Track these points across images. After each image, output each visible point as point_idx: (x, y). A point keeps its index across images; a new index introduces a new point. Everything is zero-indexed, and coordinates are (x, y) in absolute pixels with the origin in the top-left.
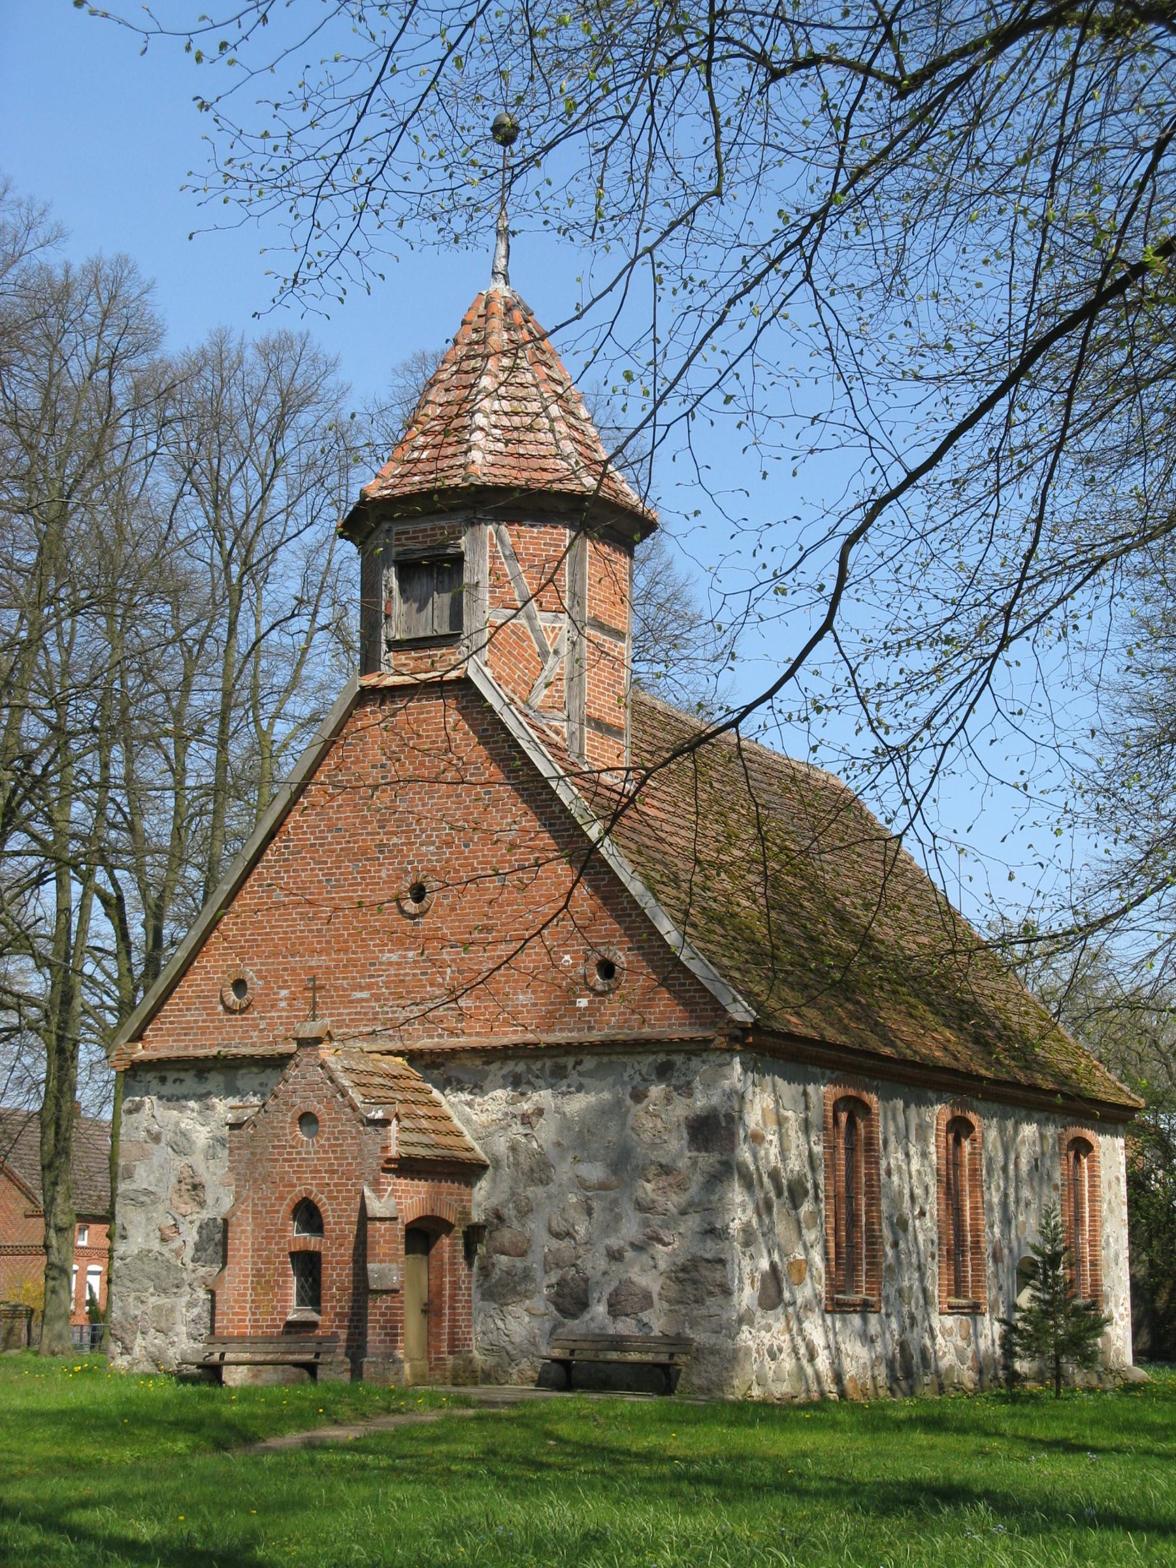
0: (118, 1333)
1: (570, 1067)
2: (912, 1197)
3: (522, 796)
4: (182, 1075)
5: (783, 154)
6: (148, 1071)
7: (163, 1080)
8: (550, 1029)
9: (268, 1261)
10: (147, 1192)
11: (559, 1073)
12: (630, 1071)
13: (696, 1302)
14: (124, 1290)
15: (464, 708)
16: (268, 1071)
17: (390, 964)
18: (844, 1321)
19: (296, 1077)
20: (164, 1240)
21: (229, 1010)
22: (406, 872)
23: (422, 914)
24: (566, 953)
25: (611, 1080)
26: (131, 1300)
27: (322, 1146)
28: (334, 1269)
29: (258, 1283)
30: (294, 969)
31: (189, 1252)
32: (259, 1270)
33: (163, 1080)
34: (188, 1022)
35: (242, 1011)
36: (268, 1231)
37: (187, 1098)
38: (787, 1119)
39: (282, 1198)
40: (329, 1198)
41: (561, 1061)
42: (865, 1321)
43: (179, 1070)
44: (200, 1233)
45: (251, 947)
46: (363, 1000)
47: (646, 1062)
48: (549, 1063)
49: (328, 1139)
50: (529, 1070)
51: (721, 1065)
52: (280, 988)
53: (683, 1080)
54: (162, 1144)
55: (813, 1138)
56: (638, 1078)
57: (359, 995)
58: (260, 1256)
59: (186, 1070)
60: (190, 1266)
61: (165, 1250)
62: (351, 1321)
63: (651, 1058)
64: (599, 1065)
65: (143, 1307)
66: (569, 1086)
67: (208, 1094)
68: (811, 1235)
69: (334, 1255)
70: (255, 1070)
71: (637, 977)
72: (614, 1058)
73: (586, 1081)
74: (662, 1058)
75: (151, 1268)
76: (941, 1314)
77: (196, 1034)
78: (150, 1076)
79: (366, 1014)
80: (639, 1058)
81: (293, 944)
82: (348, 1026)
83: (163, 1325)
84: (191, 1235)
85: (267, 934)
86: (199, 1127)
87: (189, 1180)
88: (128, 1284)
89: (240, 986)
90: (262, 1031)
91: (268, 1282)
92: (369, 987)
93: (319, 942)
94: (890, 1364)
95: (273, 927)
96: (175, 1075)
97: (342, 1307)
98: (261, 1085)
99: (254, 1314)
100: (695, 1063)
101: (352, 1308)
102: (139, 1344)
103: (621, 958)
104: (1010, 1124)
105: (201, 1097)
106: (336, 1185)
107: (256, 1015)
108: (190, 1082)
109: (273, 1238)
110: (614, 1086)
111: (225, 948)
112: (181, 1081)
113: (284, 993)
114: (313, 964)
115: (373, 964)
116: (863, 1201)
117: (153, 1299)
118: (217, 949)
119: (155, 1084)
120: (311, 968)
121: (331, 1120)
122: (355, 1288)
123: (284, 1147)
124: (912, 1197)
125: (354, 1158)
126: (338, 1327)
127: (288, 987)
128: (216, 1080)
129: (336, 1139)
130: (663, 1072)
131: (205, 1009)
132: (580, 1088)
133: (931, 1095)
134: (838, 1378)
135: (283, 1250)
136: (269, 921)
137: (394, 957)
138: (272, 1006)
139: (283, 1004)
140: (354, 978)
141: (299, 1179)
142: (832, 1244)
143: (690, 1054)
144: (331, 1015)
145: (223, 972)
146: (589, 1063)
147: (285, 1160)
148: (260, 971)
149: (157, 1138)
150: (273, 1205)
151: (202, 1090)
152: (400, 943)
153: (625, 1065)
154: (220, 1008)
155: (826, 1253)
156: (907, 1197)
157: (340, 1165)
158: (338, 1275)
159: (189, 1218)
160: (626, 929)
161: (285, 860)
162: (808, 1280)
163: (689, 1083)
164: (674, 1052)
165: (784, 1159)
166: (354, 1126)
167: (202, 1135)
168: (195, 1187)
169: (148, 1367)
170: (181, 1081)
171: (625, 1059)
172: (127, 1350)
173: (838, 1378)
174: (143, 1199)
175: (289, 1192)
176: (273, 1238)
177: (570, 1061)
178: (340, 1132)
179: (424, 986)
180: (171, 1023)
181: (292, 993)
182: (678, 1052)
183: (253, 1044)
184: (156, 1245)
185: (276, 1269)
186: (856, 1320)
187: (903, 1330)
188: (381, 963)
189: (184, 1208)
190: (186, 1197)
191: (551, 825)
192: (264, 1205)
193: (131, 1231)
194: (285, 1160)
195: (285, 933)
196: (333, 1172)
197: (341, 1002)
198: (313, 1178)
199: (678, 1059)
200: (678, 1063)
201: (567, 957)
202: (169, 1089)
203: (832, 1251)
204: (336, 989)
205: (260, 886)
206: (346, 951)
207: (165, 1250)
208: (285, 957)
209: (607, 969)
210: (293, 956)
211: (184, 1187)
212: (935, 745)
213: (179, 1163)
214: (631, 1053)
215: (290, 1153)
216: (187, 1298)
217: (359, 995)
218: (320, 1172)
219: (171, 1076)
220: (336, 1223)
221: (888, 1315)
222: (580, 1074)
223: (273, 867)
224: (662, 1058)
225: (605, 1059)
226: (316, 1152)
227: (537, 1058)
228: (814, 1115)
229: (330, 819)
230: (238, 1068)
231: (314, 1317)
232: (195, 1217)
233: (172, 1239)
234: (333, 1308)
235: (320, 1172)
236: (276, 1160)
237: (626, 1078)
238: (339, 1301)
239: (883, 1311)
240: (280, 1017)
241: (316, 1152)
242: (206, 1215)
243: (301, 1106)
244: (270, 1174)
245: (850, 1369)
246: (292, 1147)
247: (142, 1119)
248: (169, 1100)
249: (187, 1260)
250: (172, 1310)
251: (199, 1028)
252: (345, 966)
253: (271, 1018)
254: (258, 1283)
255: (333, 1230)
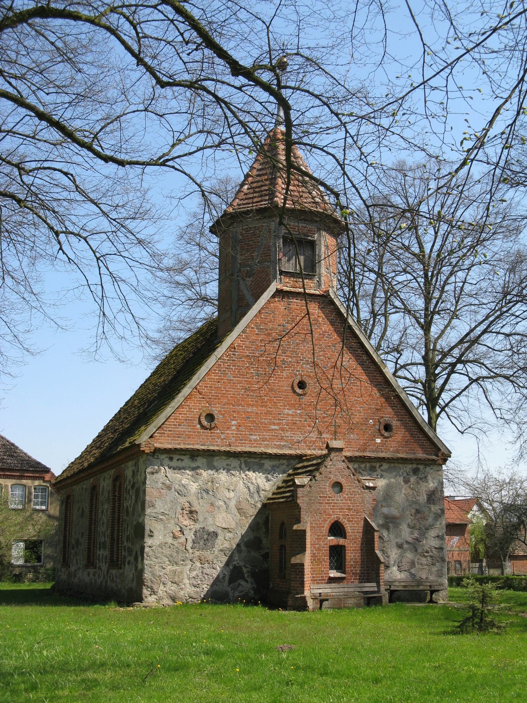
0: (149, 584)
1: (378, 467)
3: (349, 350)
4: (182, 457)
5: (251, 99)
6: (162, 454)
7: (171, 459)
8: (364, 450)
9: (319, 549)
10: (163, 514)
11: (373, 469)
12: (402, 471)
13: (433, 565)
14: (152, 562)
15: (322, 308)
16: (231, 459)
17: (288, 415)
19: (331, 465)
20: (175, 537)
21: (203, 427)
22: (296, 375)
23: (304, 394)
24: (371, 419)
25: (394, 473)
26: (157, 567)
27: (345, 497)
28: (351, 553)
29: (314, 560)
30: (239, 412)
31: (189, 545)
32: (314, 554)
33: (171, 459)
34: (180, 431)
35: (211, 429)
36: (318, 536)
37: (184, 468)
39: (325, 520)
40: (348, 521)
41: (374, 464)
43: (180, 454)
44: (195, 535)
45: (215, 399)
46: (275, 430)
47: (409, 467)
48: (368, 465)
49: (347, 494)
50: (360, 467)
51: (438, 471)
52: (231, 420)
53: (423, 476)
54: (173, 490)
56: (405, 474)
57: (273, 427)
58: (314, 547)
59: (184, 455)
60: (191, 551)
61: (175, 543)
62: (360, 576)
63: (410, 466)
64: (389, 468)
65: (164, 571)
66: (377, 475)
67: (198, 468)
69: (351, 547)
70: (224, 458)
71: (400, 434)
72: (396, 465)
73: (384, 473)
74: (415, 466)
75: (167, 551)
77: (183, 438)
78: (163, 457)
79: (277, 436)
80: (406, 465)
81: (238, 401)
82: (268, 441)
83: (176, 579)
84: (190, 536)
85: (223, 394)
86: (192, 483)
87: (187, 509)
88: (155, 560)
89: (210, 417)
90: (222, 439)
91: (319, 559)
92: (278, 424)
93: (252, 401)
95: (227, 391)
96: (178, 457)
97: (356, 570)
98: (227, 465)
99: (312, 574)
100: (428, 469)
101: (361, 570)
102: (161, 590)
103: (395, 423)
105: (193, 469)
106: (351, 515)
107: (219, 431)
108: (187, 461)
109: (321, 539)
110: (396, 476)
111: (200, 398)
112: (182, 460)
113: (234, 422)
114: (249, 410)
115: (279, 414)
117: (169, 567)
118: (195, 397)
119: (166, 461)
120: (248, 412)
121: (348, 486)
122: (362, 562)
123: (326, 497)
125: (360, 503)
126: (354, 579)
127: (237, 420)
128: (201, 461)
129: (351, 494)
130: (416, 471)
131: (189, 426)
132: (382, 476)
135: (326, 544)
136: (224, 388)
137: (290, 412)
138: (228, 428)
139: (234, 428)
140: (270, 419)
141: (333, 512)
143: (426, 465)
144: (259, 435)
145: (199, 409)
146: (385, 466)
147: (326, 503)
148: (220, 411)
149: (169, 488)
150: (320, 524)
151: (194, 465)
152: (292, 406)
153: (400, 468)
154: (199, 426)
157: (354, 506)
158: (354, 556)
159: (189, 527)
160: (396, 412)
161: (233, 360)
163: (426, 477)
164: (420, 464)
166: (359, 489)
167: (194, 487)
168: (191, 512)
169: (167, 601)
170: (182, 460)
171: (401, 466)
172: (154, 592)
174: (161, 517)
175: (328, 518)
176: (321, 539)
177: (378, 465)
178: (353, 492)
179: (305, 427)
180: (169, 431)
181: (238, 423)
182: (422, 464)
183: (218, 446)
184: (170, 540)
185: (323, 553)
188: (284, 414)
189: (186, 523)
190: (186, 517)
191: (363, 365)
192: (317, 524)
193: (156, 533)
194: (326, 503)
195: (234, 394)
196: (350, 509)
197: (264, 430)
198: (340, 512)
199: (421, 467)
200: (421, 469)
201: (371, 421)
202: (174, 463)
204: (262, 423)
205: (219, 371)
206: (266, 406)
207: (175, 543)
208: (233, 406)
209: (387, 427)
210: (238, 406)
211: (185, 512)
213: (182, 500)
214: (402, 463)
215: (328, 500)
216: (189, 567)
217: (273, 427)
218: (344, 509)
219: (176, 457)
220: (352, 532)
222: (382, 470)
223: (226, 363)
224: (415, 466)
225: (392, 465)
226: (341, 500)
227: (363, 462)
229: (257, 345)
230: (214, 456)
231: (343, 575)
232: (192, 527)
233: (180, 537)
234: (351, 570)
235: (344, 509)
236: (322, 503)
237: (401, 473)
238: (354, 567)
240: (232, 434)
241: (341, 500)
242: (198, 526)
243: (333, 478)
244: (318, 509)
246: (329, 497)
247: (160, 476)
248: (174, 469)
249: (188, 548)
250: (182, 572)
251: (186, 435)
252: (265, 413)
253: (228, 434)
254: (314, 560)
255: (350, 536)
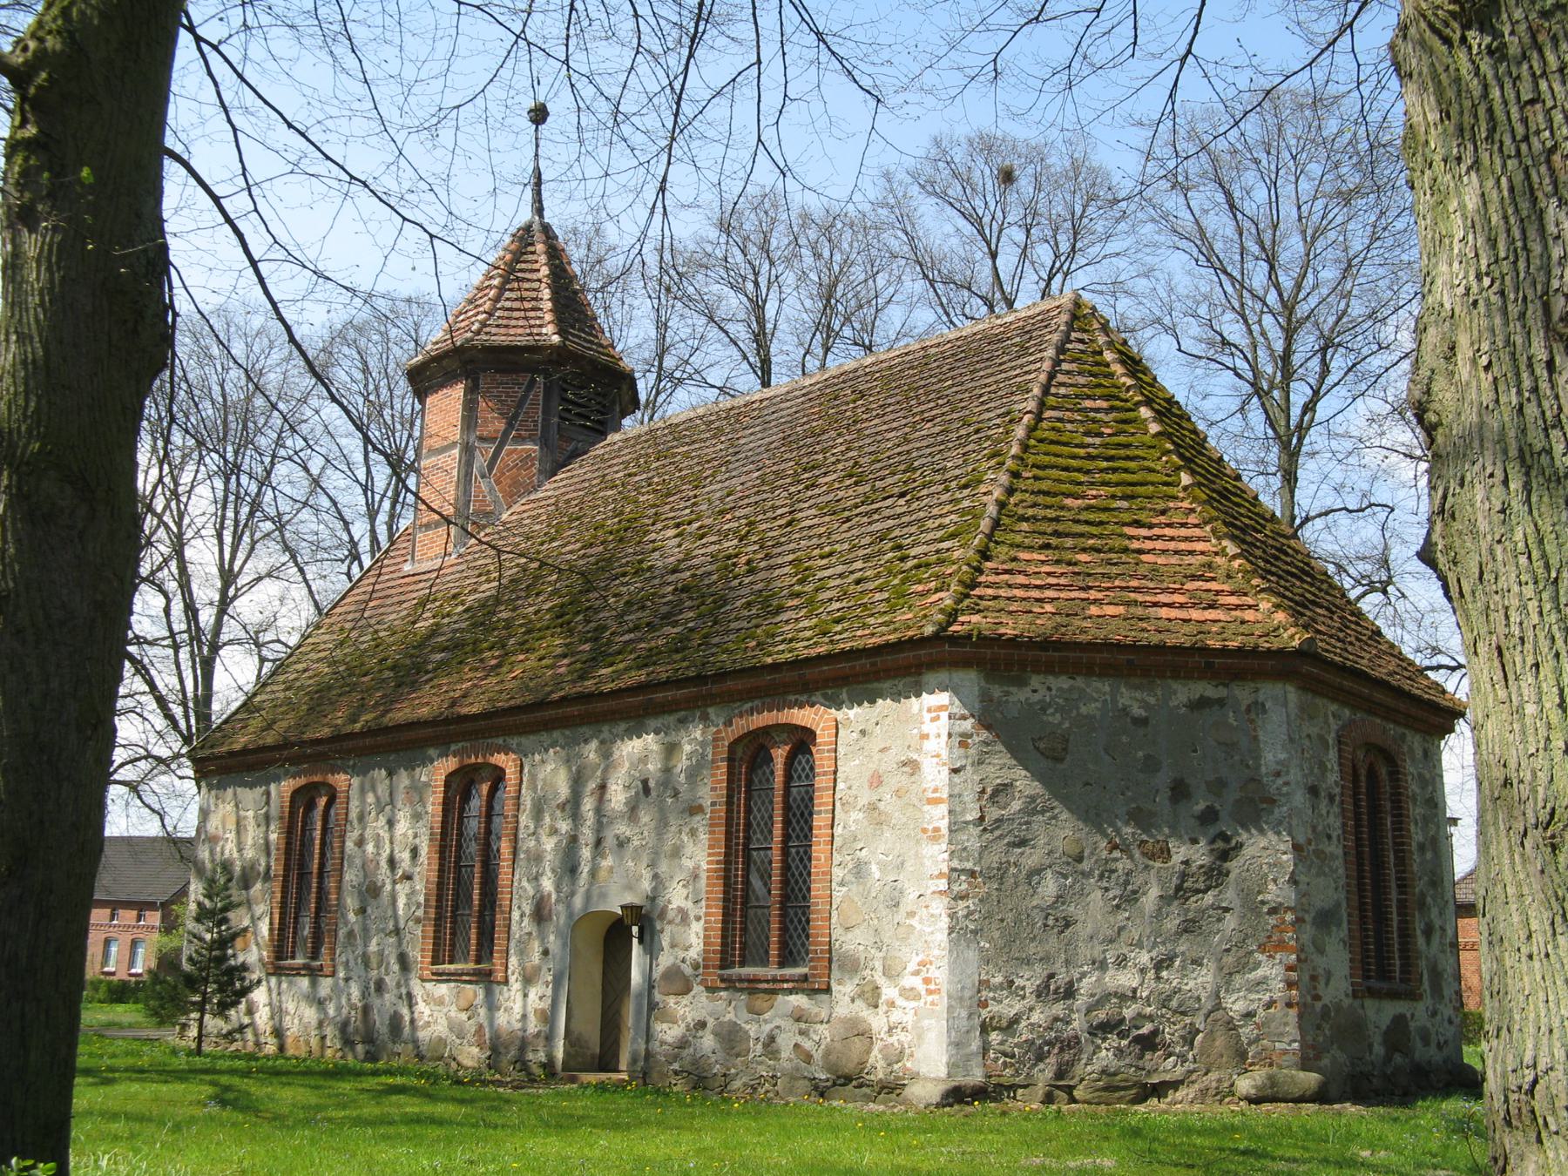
2: (392, 862)
18: (290, 983)
38: (245, 818)
42: (314, 984)
55: (272, 827)
68: (260, 909)
76: (423, 980)
94: (344, 1027)
104: (591, 751)
116: (1394, 895)
124: (392, 862)
133: (432, 752)
134: (278, 1033)
142: (277, 916)
155: (271, 923)
156: (384, 864)
162: (254, 948)
165: (240, 850)
173: (278, 1033)
186: (304, 983)
187: (365, 994)
203: (277, 921)
212: (869, 302)
221: (347, 980)
228: (274, 812)
239: (341, 975)
245: (292, 1027)
